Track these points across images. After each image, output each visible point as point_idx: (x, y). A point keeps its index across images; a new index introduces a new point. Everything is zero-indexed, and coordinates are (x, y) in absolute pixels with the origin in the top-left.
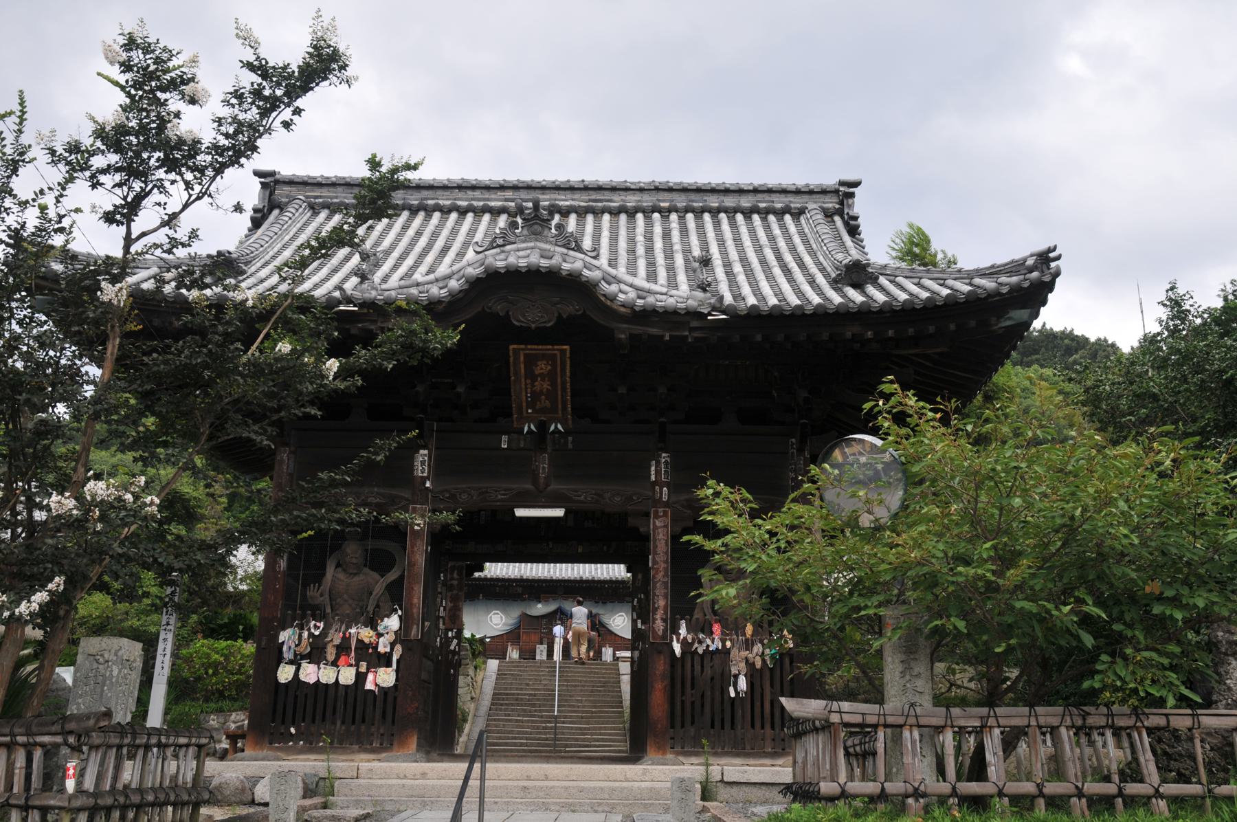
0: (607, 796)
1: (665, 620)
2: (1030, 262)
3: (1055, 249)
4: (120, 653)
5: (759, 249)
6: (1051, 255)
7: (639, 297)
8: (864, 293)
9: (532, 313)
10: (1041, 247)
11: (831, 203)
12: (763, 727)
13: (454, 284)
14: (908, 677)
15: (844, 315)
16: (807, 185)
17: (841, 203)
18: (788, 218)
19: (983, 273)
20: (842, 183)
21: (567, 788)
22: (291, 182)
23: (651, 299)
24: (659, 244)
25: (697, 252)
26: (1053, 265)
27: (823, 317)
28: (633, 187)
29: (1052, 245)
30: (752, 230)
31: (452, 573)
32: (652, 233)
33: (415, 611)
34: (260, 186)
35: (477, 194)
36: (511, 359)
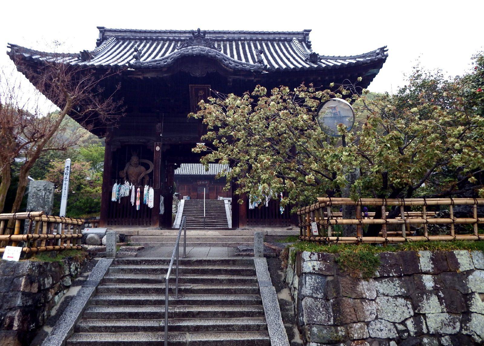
3: (386, 47)
6: (385, 49)
8: (316, 64)
13: (169, 60)
15: (311, 69)
17: (305, 38)
19: (360, 57)
20: (305, 31)
22: (110, 31)
26: (385, 53)
34: (99, 32)
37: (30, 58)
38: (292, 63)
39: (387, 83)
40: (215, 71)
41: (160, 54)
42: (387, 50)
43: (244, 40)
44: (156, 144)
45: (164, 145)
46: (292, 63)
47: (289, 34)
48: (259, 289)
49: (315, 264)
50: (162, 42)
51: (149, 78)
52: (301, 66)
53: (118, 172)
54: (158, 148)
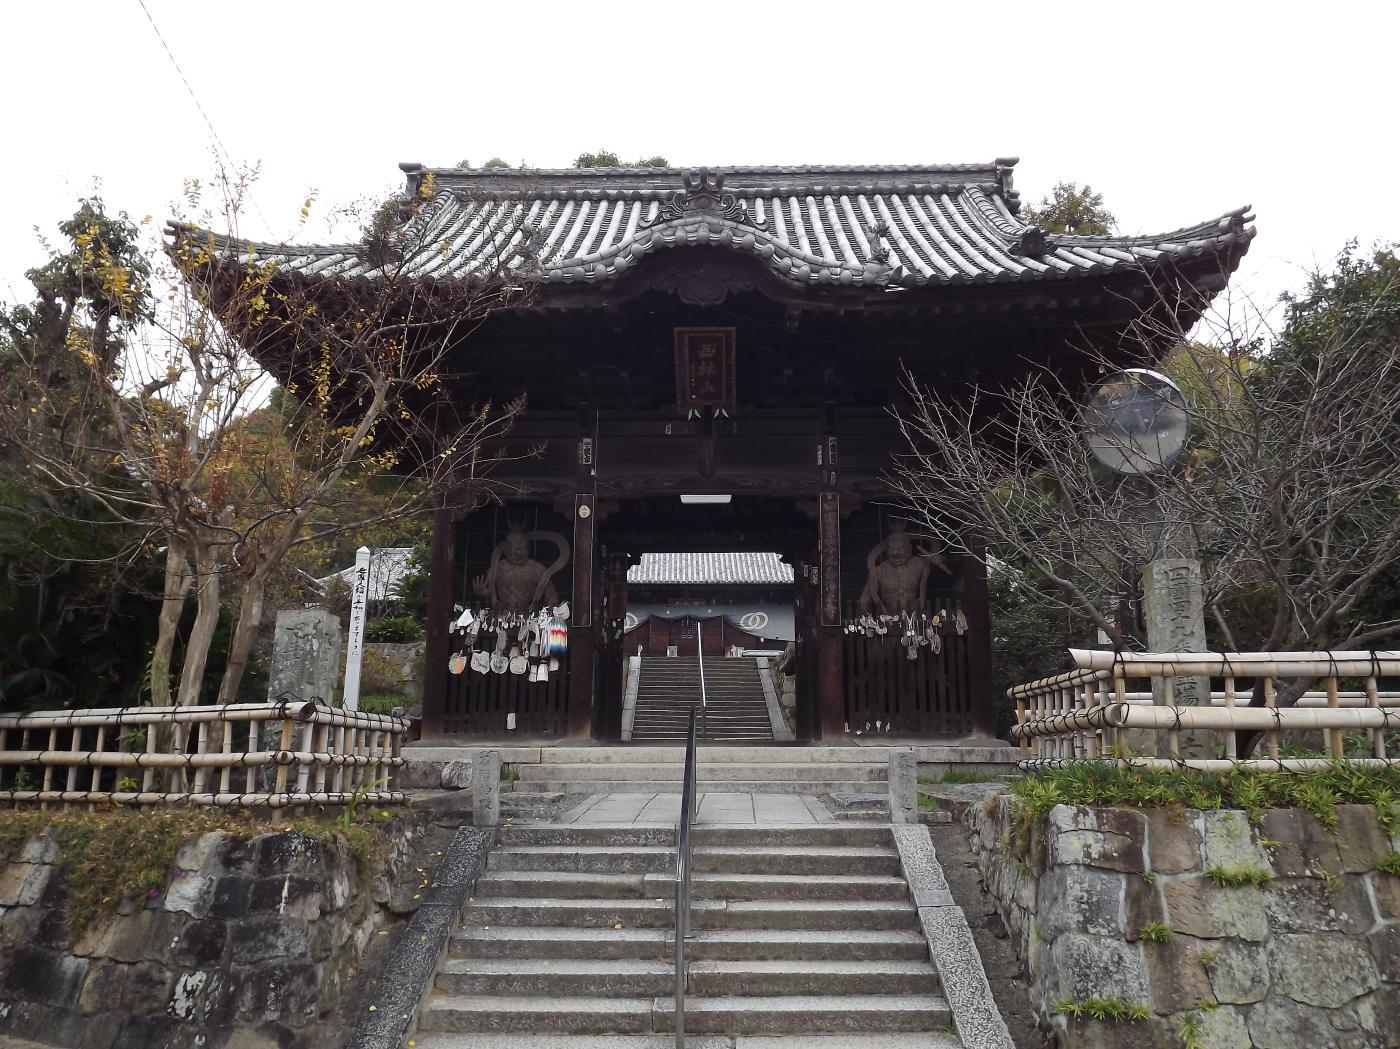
0: (795, 777)
1: (835, 604)
2: (1224, 223)
4: (320, 626)
5: (921, 228)
6: (1245, 216)
7: (812, 271)
9: (702, 291)
10: (1237, 207)
11: (990, 183)
12: (938, 709)
14: (1180, 637)
15: (1029, 281)
16: (963, 165)
17: (1000, 182)
18: (945, 198)
20: (1000, 162)
21: (754, 770)
23: (825, 272)
24: (818, 226)
25: (873, 222)
27: (1005, 285)
28: (784, 171)
29: (1248, 205)
30: (911, 211)
31: (614, 564)
32: (808, 215)
33: (585, 599)
35: (626, 182)
36: (676, 342)
37: (231, 262)
38: (976, 265)
39: (1247, 313)
40: (751, 289)
41: (588, 242)
42: (1253, 218)
43: (841, 193)
44: (580, 498)
45: (600, 500)
46: (976, 265)
47: (953, 172)
48: (917, 914)
49: (1091, 841)
50: (506, 204)
51: (563, 310)
52: (979, 271)
53: (470, 582)
54: (585, 512)
